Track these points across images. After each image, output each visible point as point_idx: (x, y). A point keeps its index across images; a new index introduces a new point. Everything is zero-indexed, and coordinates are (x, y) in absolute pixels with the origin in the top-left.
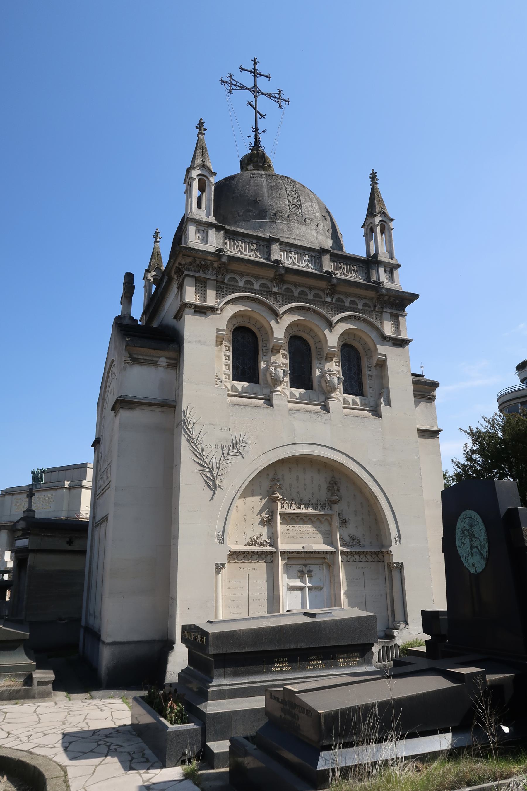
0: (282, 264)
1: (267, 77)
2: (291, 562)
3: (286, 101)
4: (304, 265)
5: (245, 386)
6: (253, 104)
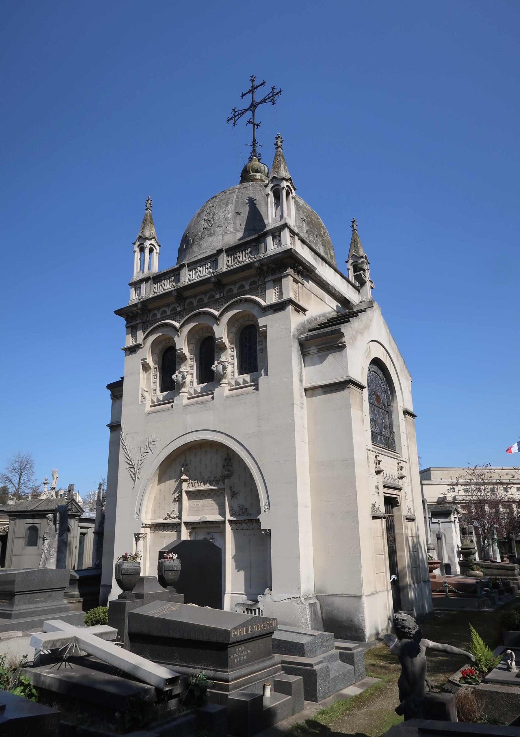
2: (197, 531)
4: (204, 272)
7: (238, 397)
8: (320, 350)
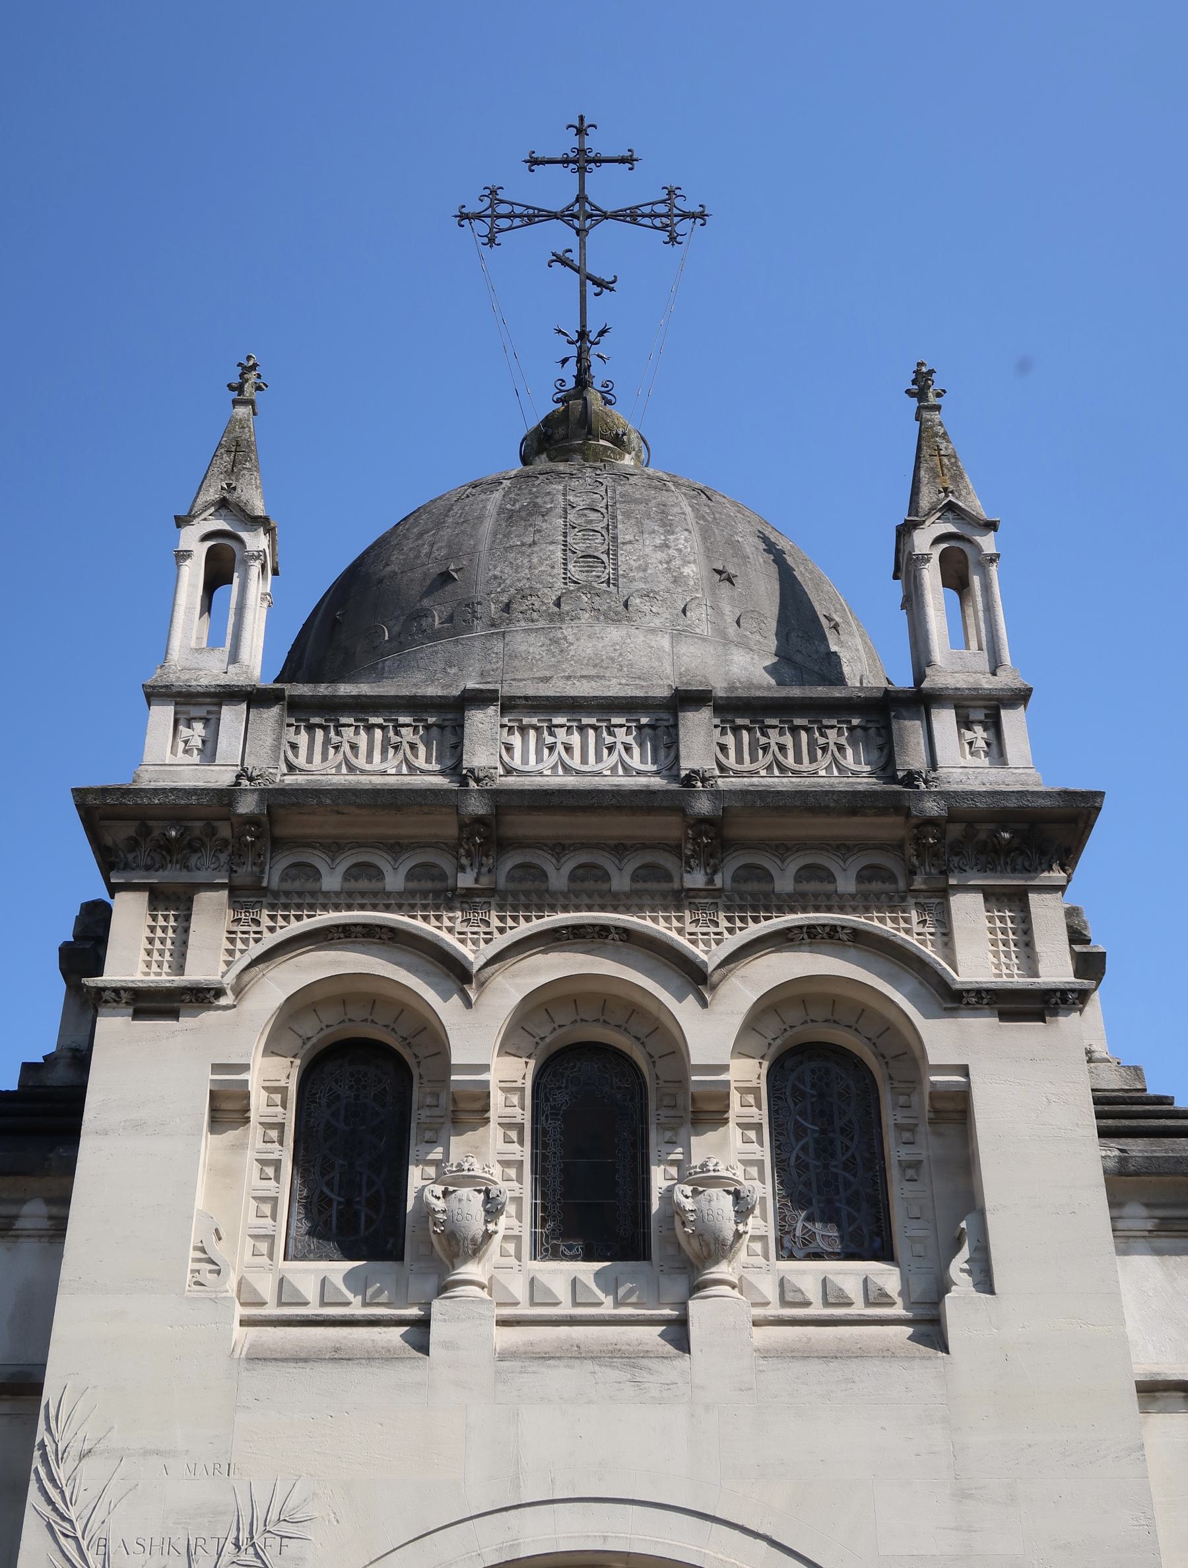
0: (704, 780)
1: (622, 160)
3: (693, 216)
4: (614, 763)
6: (574, 257)
7: (834, 1364)
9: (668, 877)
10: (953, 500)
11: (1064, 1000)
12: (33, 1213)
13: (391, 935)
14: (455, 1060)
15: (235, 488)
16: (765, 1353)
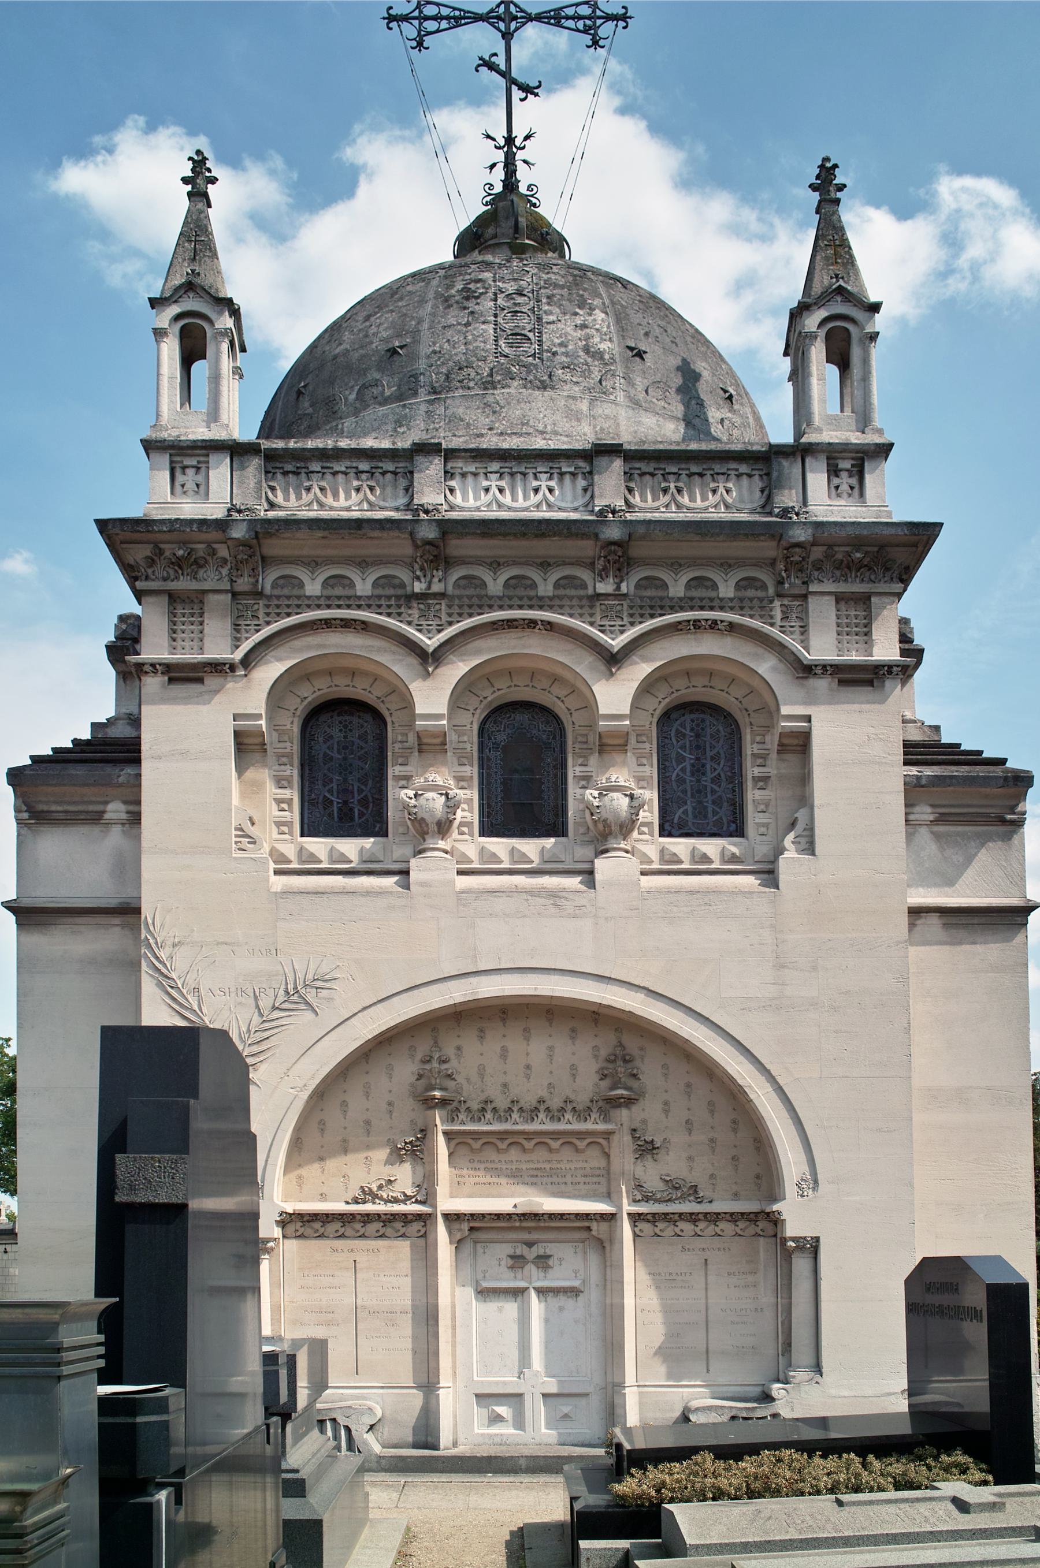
0: (614, 512)
5: (548, 846)
6: (501, 61)
8: (942, 819)
9: (584, 586)
10: (843, 284)
11: (890, 672)
12: (116, 810)
13: (363, 626)
14: (419, 710)
15: (199, 274)
16: (287, 893)
